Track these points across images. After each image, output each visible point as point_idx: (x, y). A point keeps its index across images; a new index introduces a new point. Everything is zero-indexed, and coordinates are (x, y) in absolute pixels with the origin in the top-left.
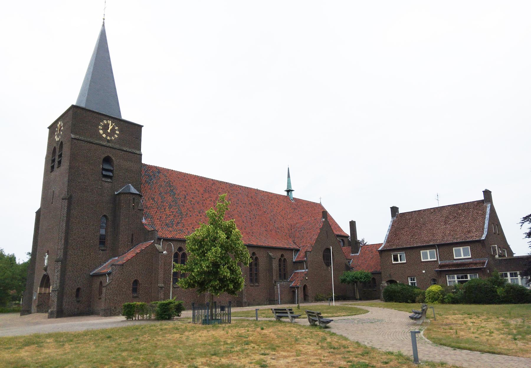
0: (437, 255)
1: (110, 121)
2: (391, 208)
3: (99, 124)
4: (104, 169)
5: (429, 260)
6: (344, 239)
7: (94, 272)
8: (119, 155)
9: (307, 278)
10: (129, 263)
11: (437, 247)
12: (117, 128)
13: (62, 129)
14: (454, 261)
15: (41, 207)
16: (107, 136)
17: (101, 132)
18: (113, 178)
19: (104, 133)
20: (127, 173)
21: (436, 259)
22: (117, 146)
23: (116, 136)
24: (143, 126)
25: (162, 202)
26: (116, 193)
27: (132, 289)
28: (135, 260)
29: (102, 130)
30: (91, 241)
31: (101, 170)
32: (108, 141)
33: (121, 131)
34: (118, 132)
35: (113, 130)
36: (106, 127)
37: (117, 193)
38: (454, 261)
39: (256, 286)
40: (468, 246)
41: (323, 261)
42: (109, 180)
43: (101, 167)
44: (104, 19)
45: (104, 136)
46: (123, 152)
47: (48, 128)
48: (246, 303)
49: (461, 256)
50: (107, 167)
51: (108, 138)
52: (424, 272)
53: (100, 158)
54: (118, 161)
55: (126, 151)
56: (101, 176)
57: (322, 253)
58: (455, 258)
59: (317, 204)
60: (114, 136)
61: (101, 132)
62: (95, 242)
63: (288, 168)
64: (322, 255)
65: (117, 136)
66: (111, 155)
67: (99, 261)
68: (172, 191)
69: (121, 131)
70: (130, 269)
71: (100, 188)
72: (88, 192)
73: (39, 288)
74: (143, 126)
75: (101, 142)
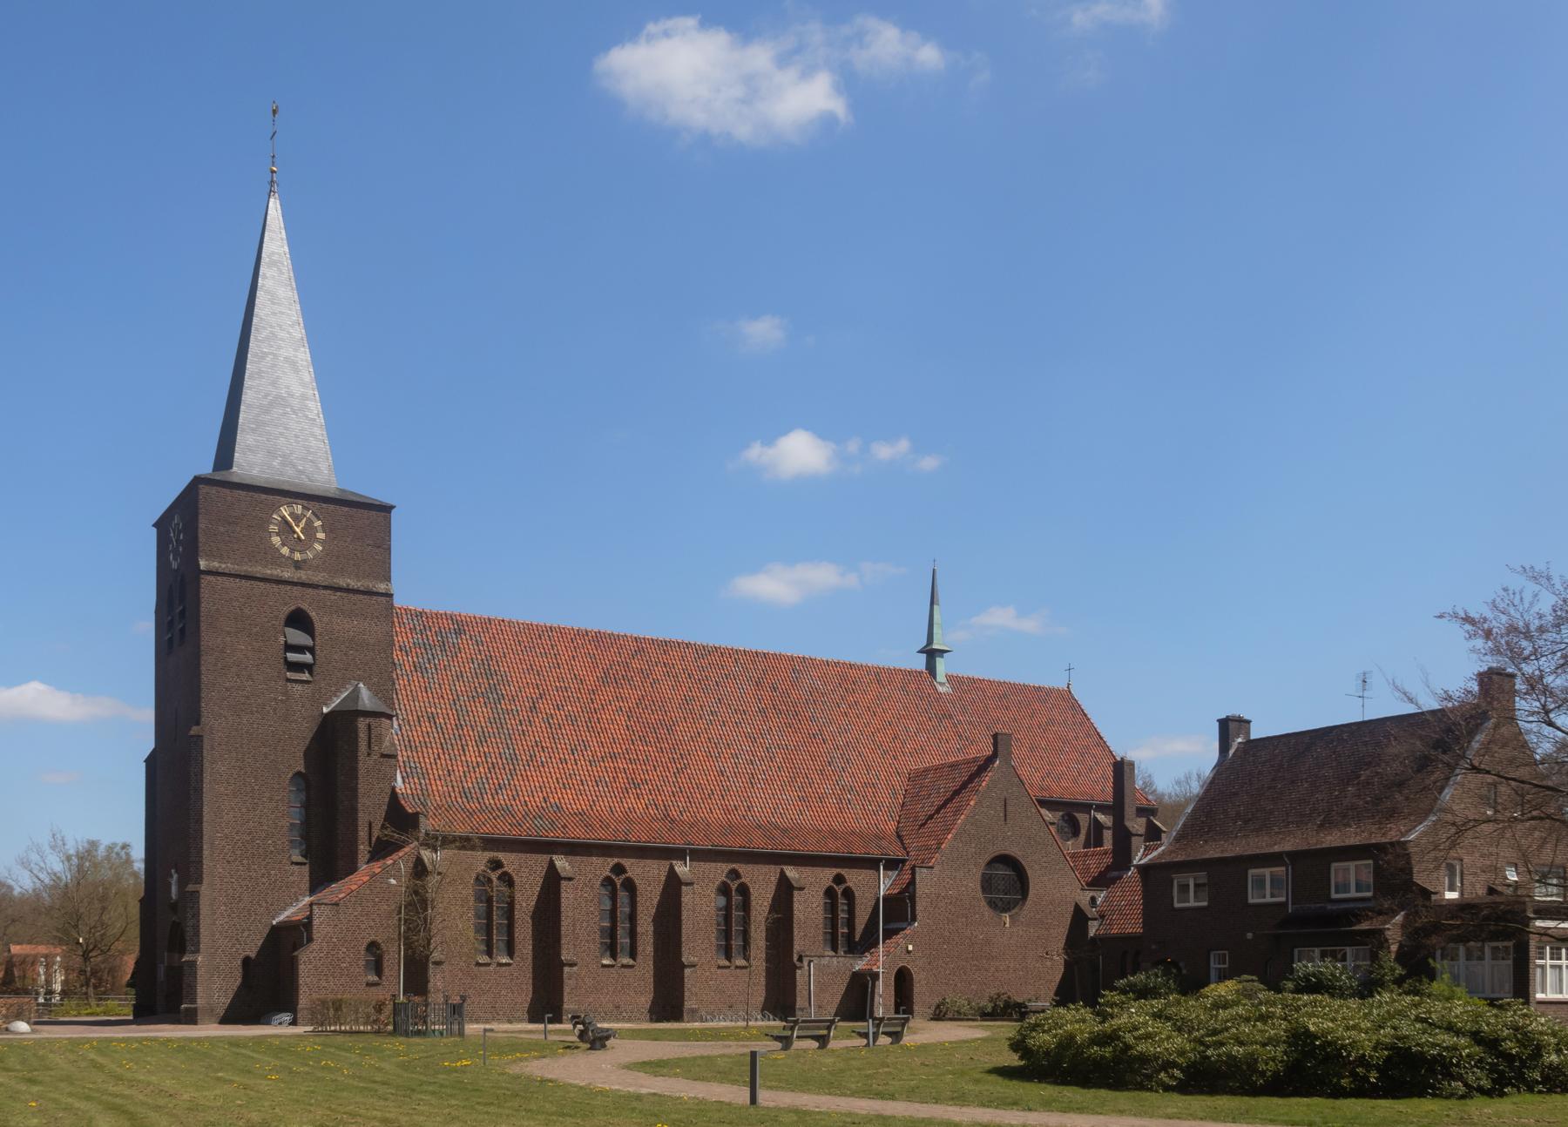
0: (1287, 884)
1: (300, 507)
2: (1218, 720)
3: (269, 521)
4: (290, 648)
5: (1268, 899)
6: (740, 871)
7: (282, 918)
8: (329, 604)
9: (910, 948)
10: (353, 899)
11: (1286, 859)
12: (318, 523)
13: (181, 537)
14: (1329, 907)
15: (156, 746)
16: (292, 551)
17: (276, 540)
18: (316, 669)
19: (283, 545)
20: (351, 652)
21: (1283, 899)
22: (320, 578)
23: (319, 547)
24: (393, 507)
25: (459, 726)
26: (325, 710)
27: (364, 963)
28: (368, 892)
29: (278, 534)
30: (270, 842)
31: (282, 652)
32: (298, 565)
33: (331, 531)
34: (321, 535)
35: (309, 529)
36: (286, 528)
37: (330, 709)
38: (1329, 907)
39: (737, 967)
40: (1329, 869)
41: (980, 895)
42: (306, 676)
43: (282, 642)
44: (273, 157)
45: (285, 551)
46: (339, 594)
47: (154, 526)
48: (693, 1011)
49: (1189, 902)
50: (297, 637)
51: (297, 556)
52: (1250, 936)
53: (276, 617)
54: (325, 619)
55: (348, 590)
56: (282, 667)
57: (976, 873)
58: (1334, 896)
59: (1049, 692)
61: (276, 540)
62: (279, 842)
63: (934, 570)
64: (978, 876)
65: (321, 548)
66: (305, 606)
67: (293, 890)
68: (493, 688)
69: (331, 531)
70: (356, 913)
71: (281, 700)
72: (252, 713)
73: (166, 954)
74: (393, 507)
75: (276, 572)
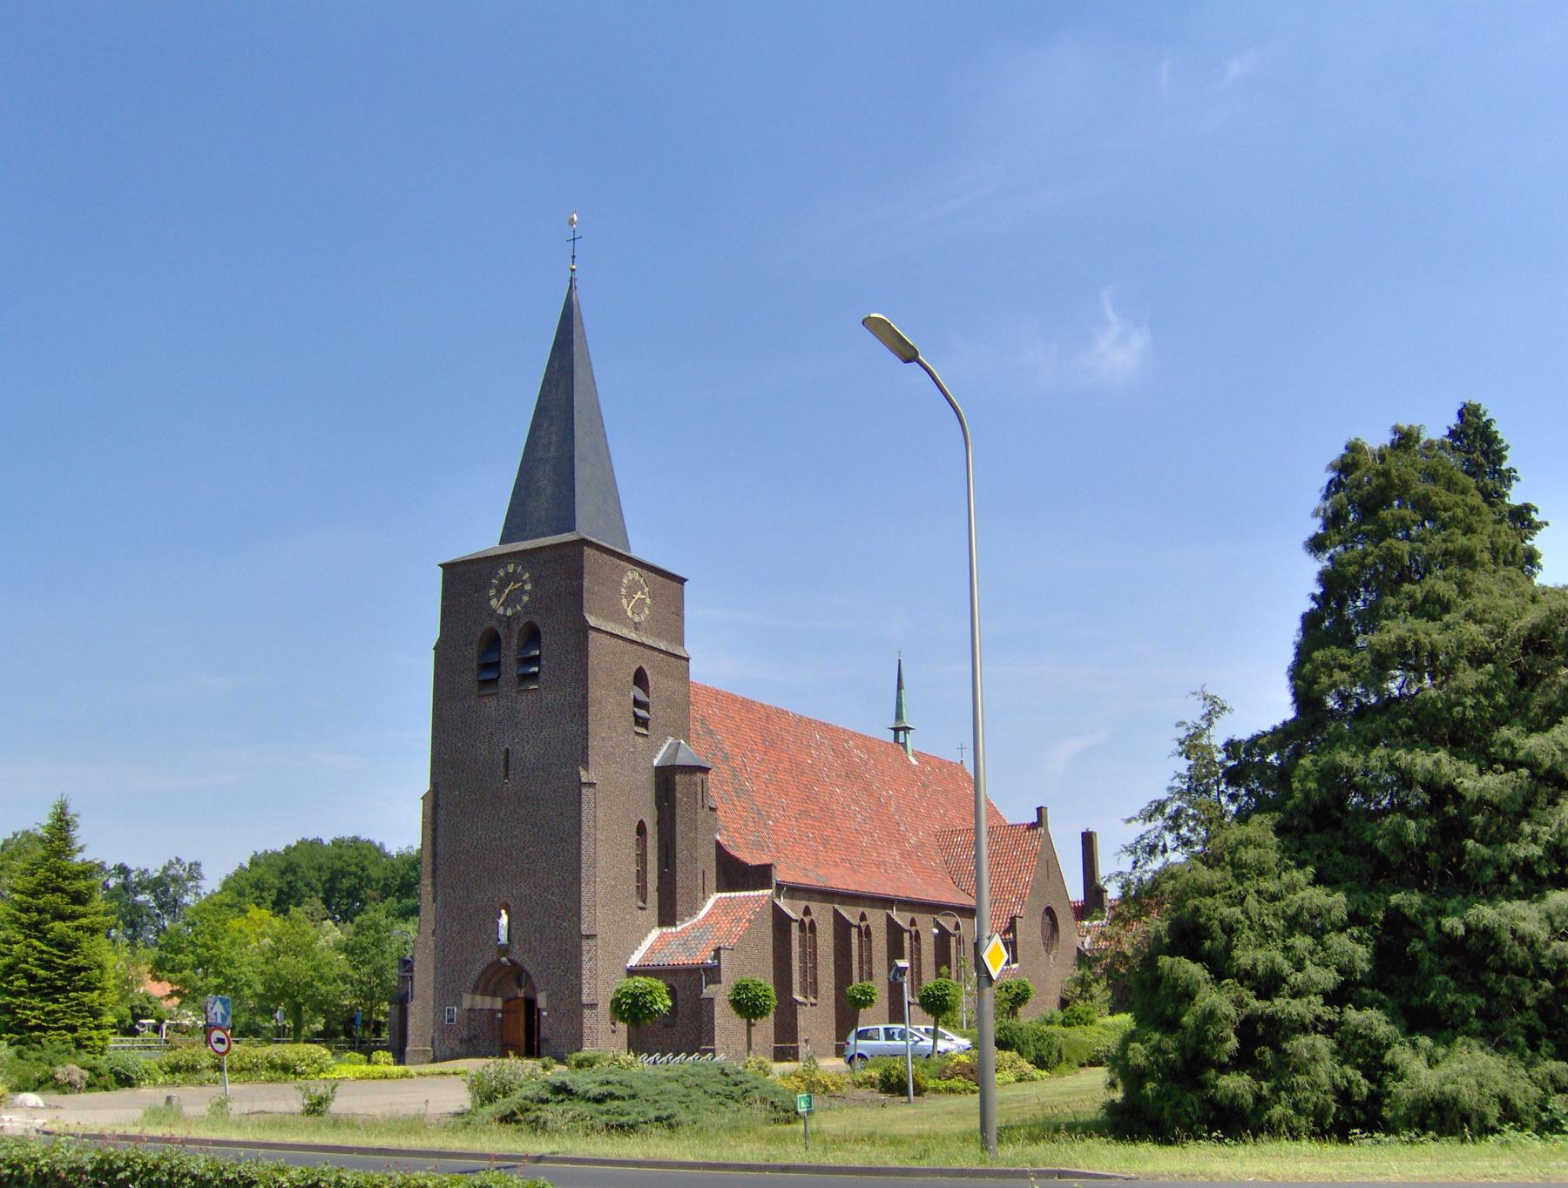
60: (520, 601)
